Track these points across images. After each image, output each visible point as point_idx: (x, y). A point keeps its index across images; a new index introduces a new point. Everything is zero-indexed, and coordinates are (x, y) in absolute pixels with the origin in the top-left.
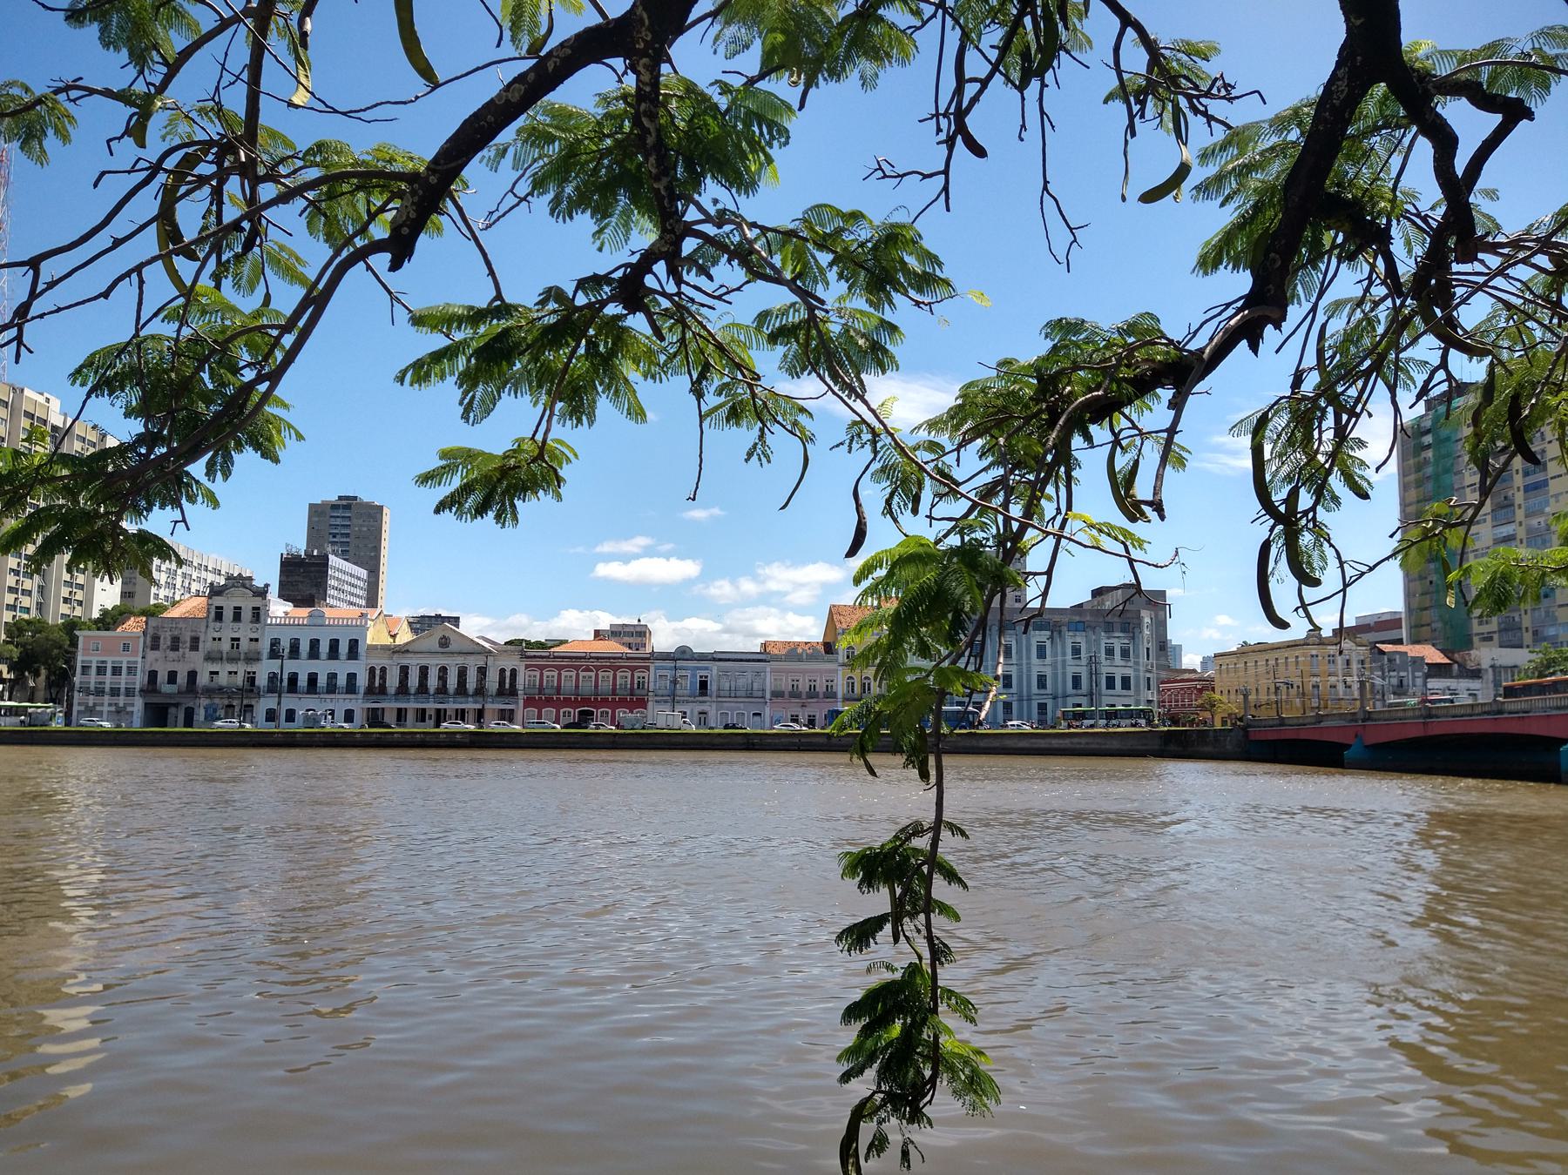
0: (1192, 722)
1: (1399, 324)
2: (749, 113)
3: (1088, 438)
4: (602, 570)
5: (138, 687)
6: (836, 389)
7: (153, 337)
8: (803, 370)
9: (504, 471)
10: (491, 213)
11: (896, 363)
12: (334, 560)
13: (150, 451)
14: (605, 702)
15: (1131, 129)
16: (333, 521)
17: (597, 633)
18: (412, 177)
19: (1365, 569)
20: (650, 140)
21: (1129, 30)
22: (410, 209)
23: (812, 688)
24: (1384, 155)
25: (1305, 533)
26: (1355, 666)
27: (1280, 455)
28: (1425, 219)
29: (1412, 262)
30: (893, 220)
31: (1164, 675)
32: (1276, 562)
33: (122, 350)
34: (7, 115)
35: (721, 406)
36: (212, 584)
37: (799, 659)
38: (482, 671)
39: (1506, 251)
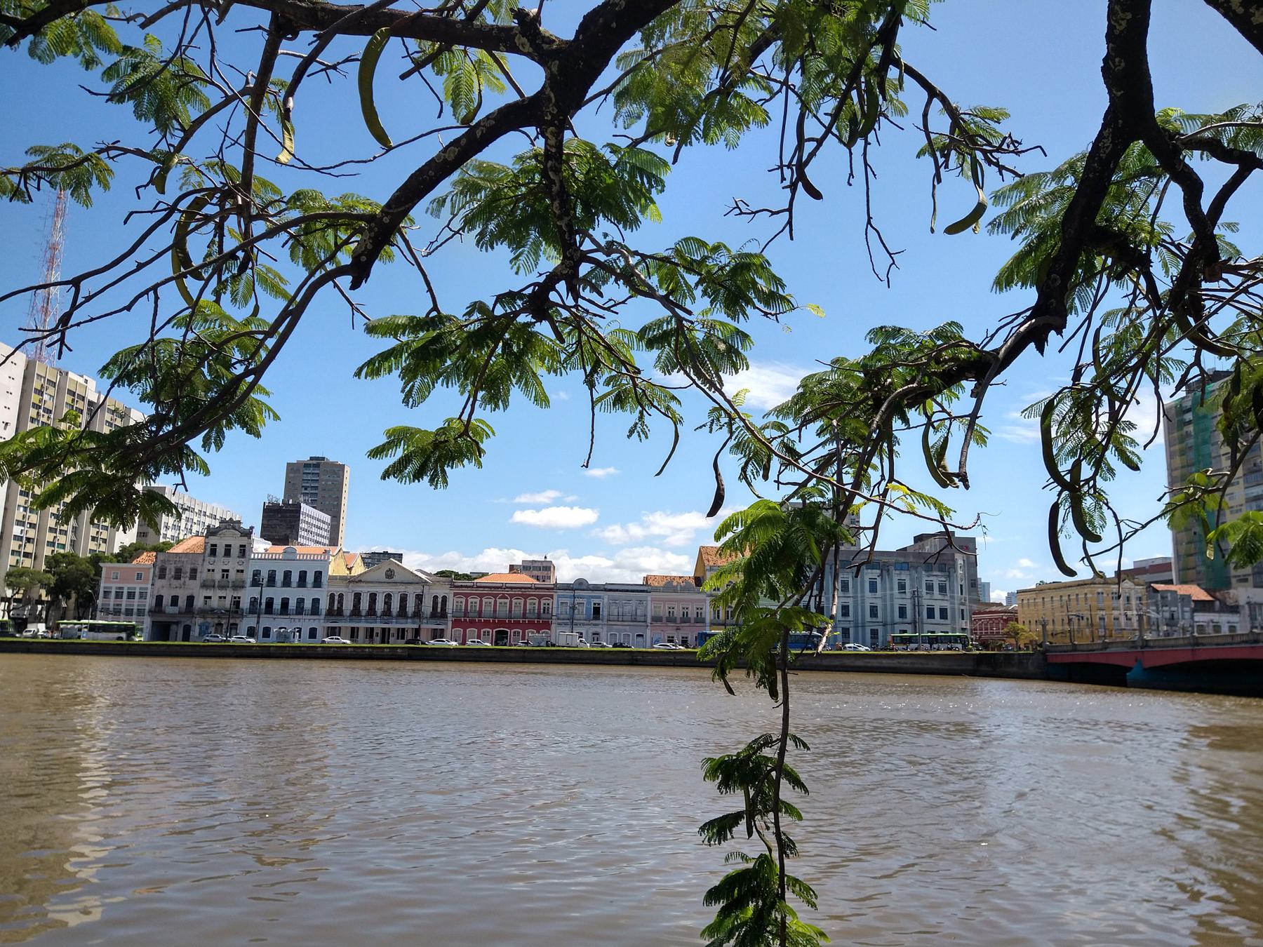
0: (1000, 647)
1: (1159, 331)
2: (633, 167)
3: (905, 420)
4: (519, 517)
5: (147, 608)
6: (699, 383)
7: (164, 341)
8: (673, 368)
9: (437, 445)
10: (432, 243)
11: (747, 363)
12: (305, 508)
13: (160, 428)
14: (517, 624)
15: (938, 177)
16: (305, 477)
17: (512, 568)
18: (370, 218)
19: (1138, 527)
20: (555, 189)
21: (936, 101)
22: (367, 242)
23: (685, 615)
24: (1143, 196)
25: (1087, 498)
26: (1134, 602)
27: (1065, 434)
28: (1178, 246)
29: (1168, 281)
30: (745, 251)
31: (975, 607)
32: (1064, 521)
33: (140, 350)
34: (62, 170)
35: (609, 394)
36: (209, 526)
37: (675, 590)
38: (419, 598)
39: (1245, 272)
